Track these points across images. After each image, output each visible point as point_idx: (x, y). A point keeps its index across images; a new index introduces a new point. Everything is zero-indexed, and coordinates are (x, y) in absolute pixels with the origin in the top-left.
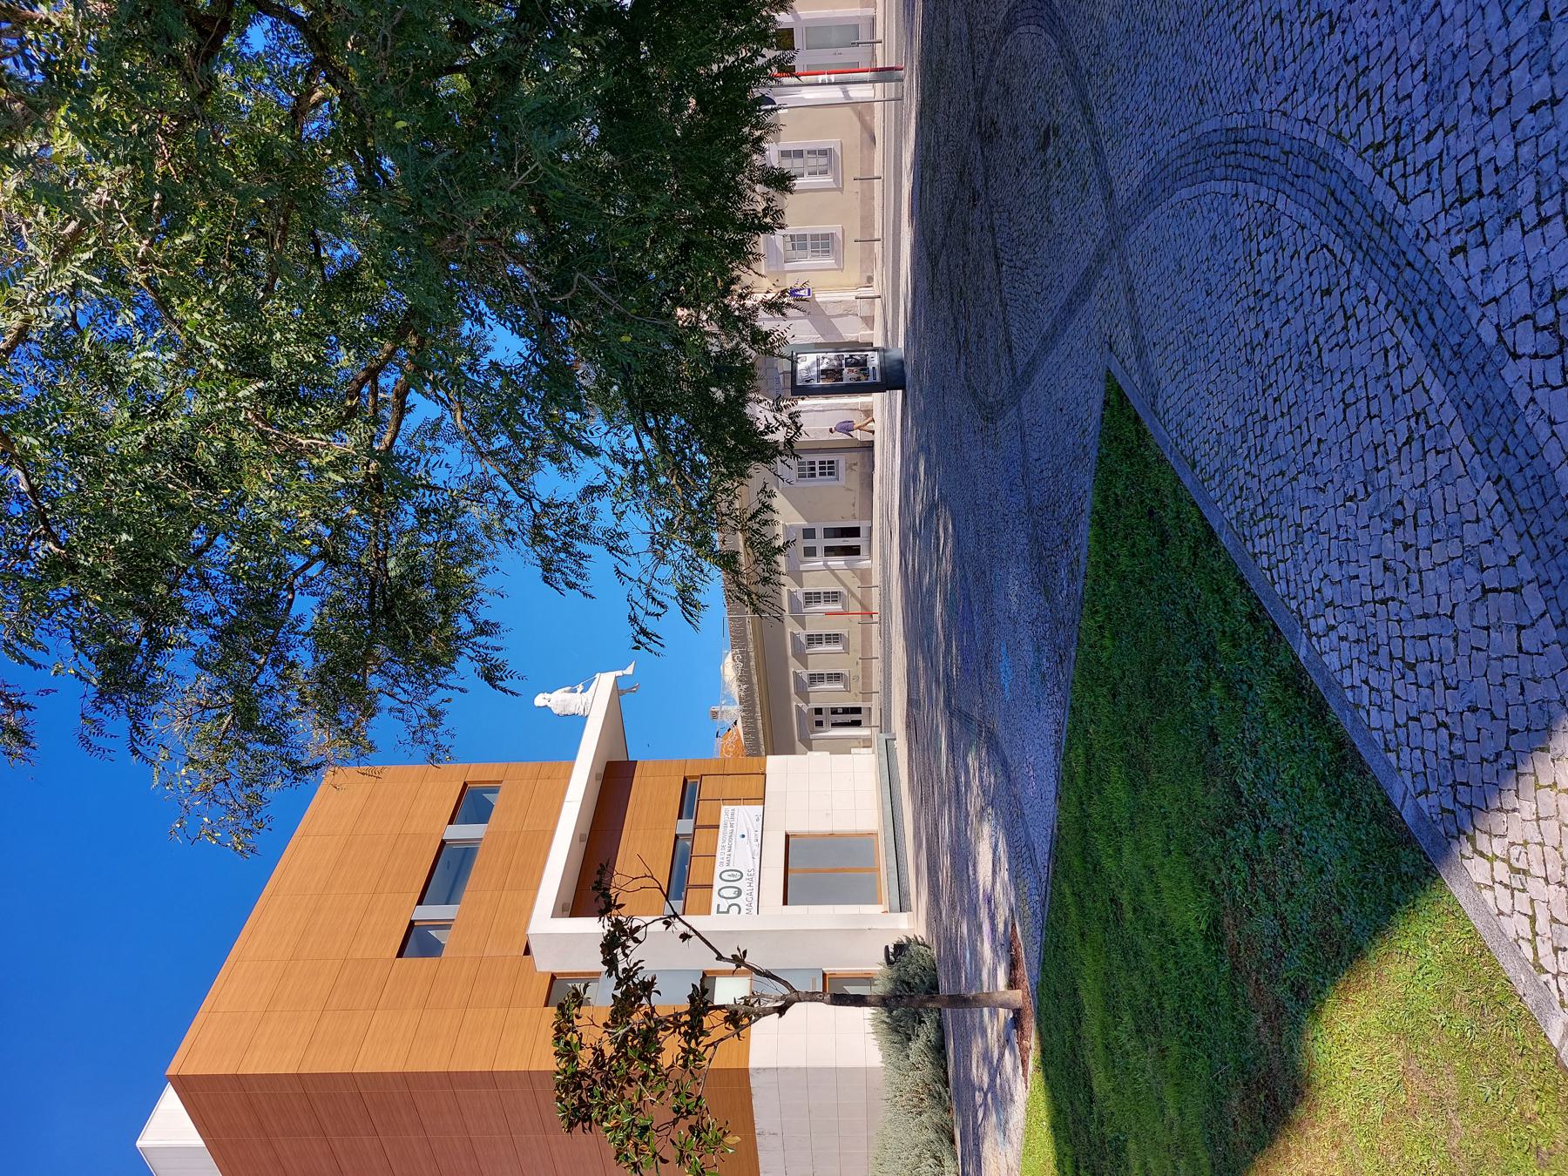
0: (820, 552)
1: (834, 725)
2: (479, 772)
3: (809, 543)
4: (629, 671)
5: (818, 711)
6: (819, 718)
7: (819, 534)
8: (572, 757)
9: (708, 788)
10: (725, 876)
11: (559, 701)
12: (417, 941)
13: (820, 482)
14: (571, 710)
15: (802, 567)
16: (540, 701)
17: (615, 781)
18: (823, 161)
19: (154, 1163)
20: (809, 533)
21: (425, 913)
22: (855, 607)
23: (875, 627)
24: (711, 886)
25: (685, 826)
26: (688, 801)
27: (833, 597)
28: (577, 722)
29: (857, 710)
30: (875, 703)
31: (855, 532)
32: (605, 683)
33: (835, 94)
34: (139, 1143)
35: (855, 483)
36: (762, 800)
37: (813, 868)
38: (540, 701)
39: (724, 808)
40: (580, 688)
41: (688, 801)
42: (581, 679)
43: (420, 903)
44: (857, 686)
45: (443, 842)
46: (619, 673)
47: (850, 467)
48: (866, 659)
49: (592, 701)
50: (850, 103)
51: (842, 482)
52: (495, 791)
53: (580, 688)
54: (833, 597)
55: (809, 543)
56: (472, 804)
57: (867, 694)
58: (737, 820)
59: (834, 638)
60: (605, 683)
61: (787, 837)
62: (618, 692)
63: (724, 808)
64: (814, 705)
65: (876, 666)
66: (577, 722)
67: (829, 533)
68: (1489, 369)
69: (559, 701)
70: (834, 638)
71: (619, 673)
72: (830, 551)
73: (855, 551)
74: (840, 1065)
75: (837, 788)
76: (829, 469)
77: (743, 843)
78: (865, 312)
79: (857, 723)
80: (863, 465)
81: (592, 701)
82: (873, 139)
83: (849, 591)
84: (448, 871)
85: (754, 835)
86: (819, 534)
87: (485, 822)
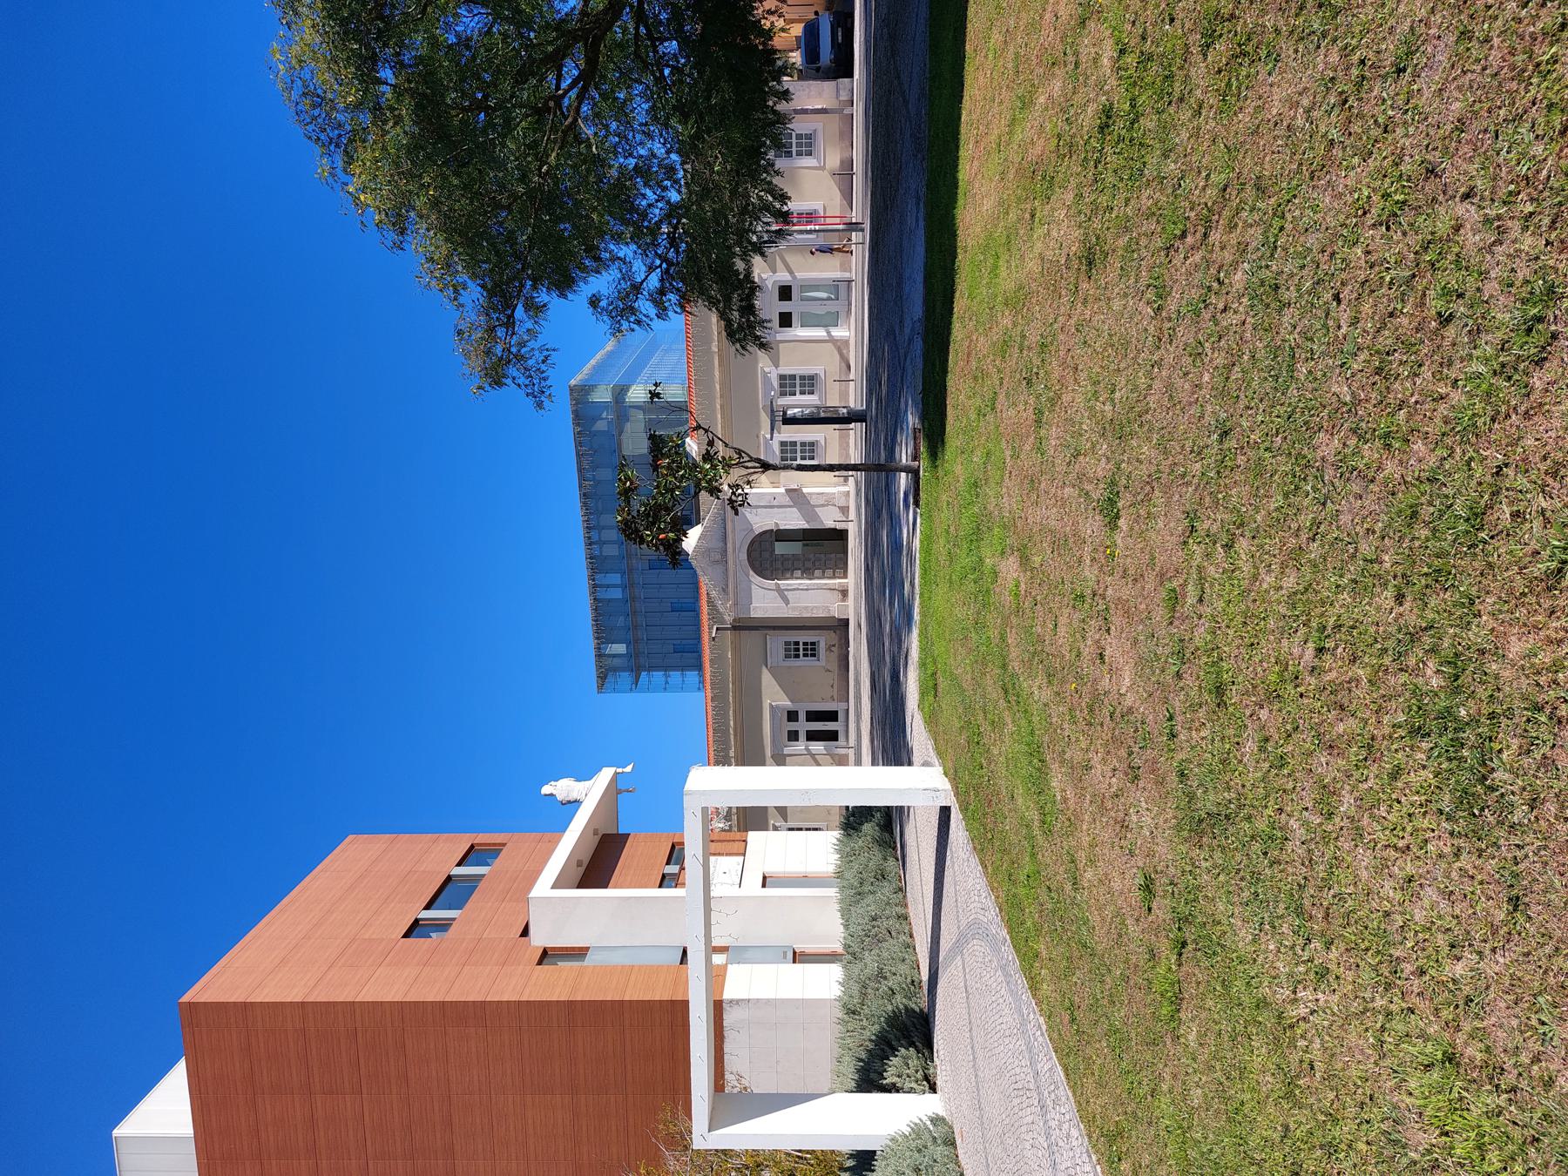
0: (802, 736)
3: (793, 726)
4: (629, 769)
7: (802, 716)
11: (563, 788)
13: (804, 662)
15: (787, 751)
16: (546, 790)
18: (826, 54)
19: (127, 1161)
20: (792, 716)
31: (832, 716)
33: (819, 333)
34: (116, 1132)
35: (834, 666)
38: (546, 790)
42: (584, 775)
47: (829, 649)
49: (589, 792)
50: (832, 340)
51: (823, 663)
55: (793, 726)
60: (606, 774)
66: (575, 804)
67: (813, 716)
68: (1356, 1006)
69: (563, 788)
72: (813, 736)
73: (832, 736)
76: (811, 650)
78: (842, 503)
80: (840, 647)
82: (849, 367)
86: (802, 716)
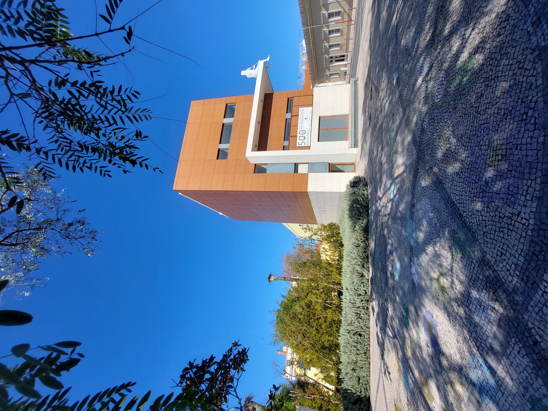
1: (336, 61)
2: (230, 100)
4: (268, 59)
5: (331, 58)
6: (331, 59)
8: (253, 92)
9: (295, 102)
10: (300, 138)
11: (247, 73)
12: (221, 154)
14: (252, 76)
16: (243, 73)
17: (267, 100)
21: (222, 146)
22: (346, 19)
23: (352, 27)
24: (296, 136)
25: (289, 116)
26: (289, 108)
27: (338, 14)
28: (254, 80)
29: (344, 56)
30: (350, 55)
32: (261, 64)
36: (311, 105)
37: (329, 129)
38: (243, 73)
39: (300, 109)
40: (254, 67)
41: (289, 108)
42: (252, 64)
43: (220, 143)
44: (344, 48)
45: (223, 124)
46: (265, 60)
48: (348, 40)
49: (256, 72)
52: (235, 106)
53: (254, 67)
54: (338, 14)
56: (229, 111)
57: (347, 51)
58: (304, 113)
59: (338, 31)
60: (261, 64)
61: (320, 117)
62: (266, 67)
63: (300, 109)
64: (330, 56)
65: (351, 42)
66: (254, 80)
69: (247, 73)
70: (338, 31)
71: (265, 60)
74: (333, 191)
75: (335, 97)
77: (306, 121)
79: (343, 60)
81: (256, 72)
83: (344, 11)
84: (225, 132)
85: (309, 118)
87: (233, 117)
